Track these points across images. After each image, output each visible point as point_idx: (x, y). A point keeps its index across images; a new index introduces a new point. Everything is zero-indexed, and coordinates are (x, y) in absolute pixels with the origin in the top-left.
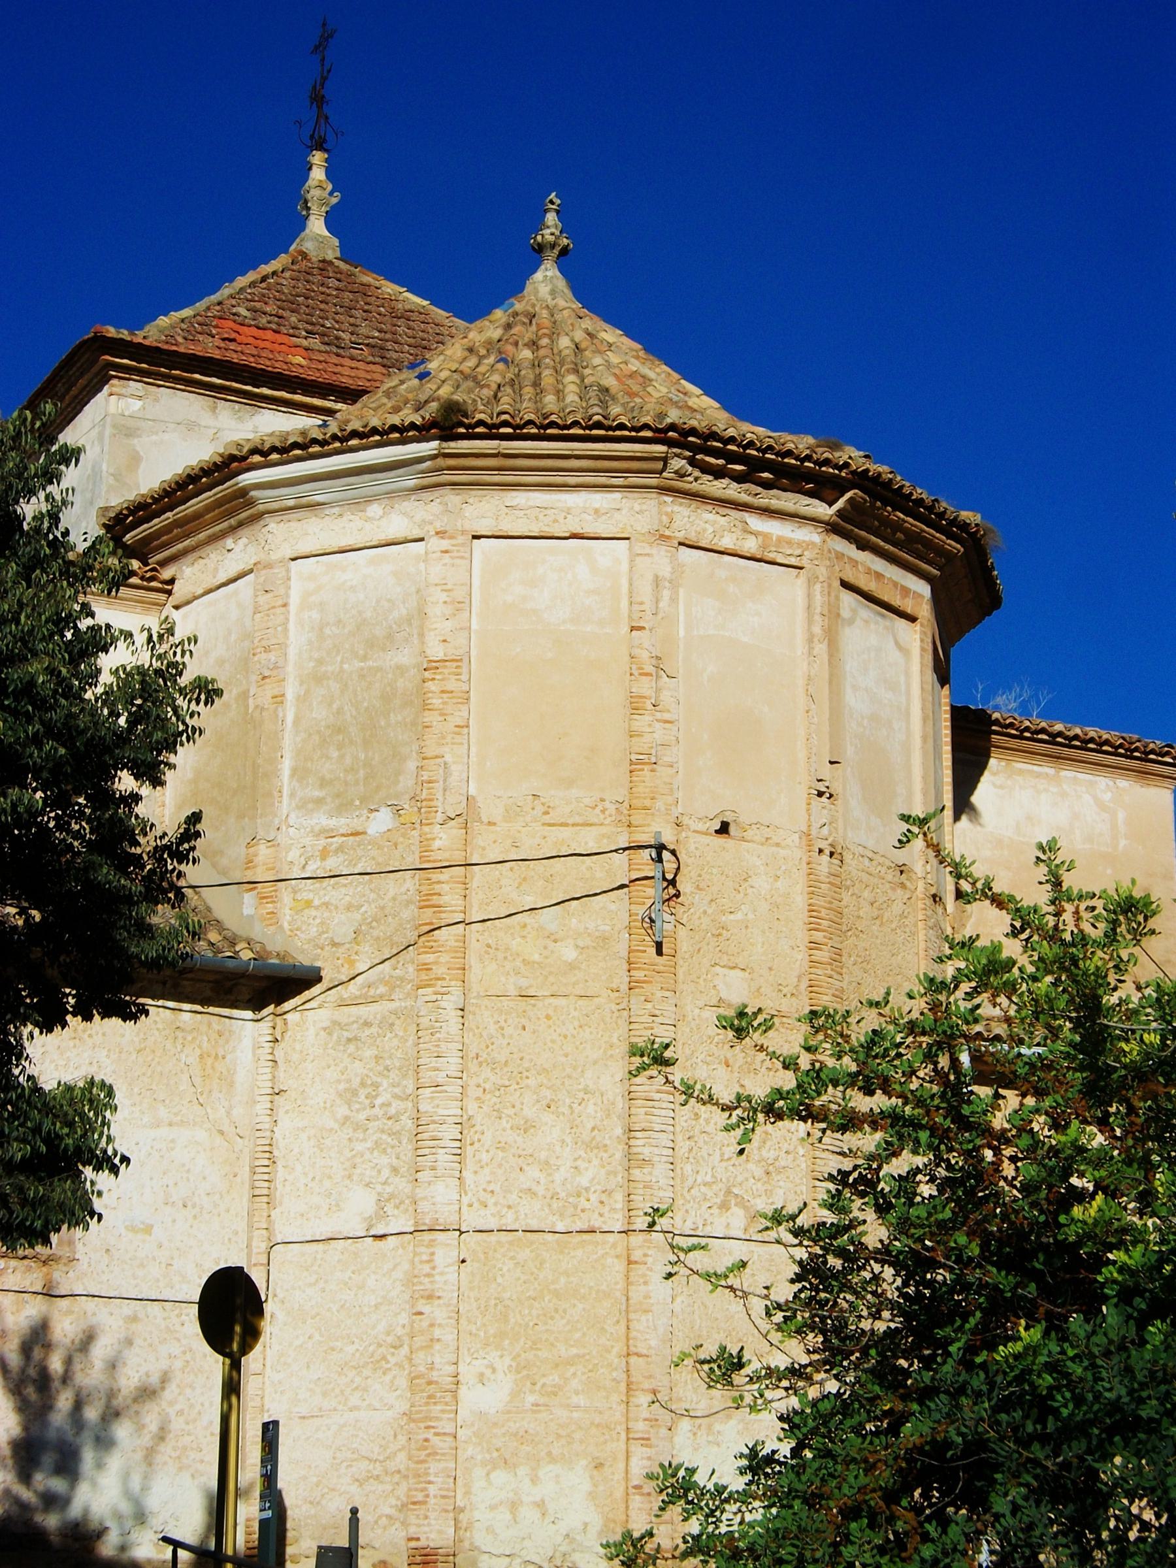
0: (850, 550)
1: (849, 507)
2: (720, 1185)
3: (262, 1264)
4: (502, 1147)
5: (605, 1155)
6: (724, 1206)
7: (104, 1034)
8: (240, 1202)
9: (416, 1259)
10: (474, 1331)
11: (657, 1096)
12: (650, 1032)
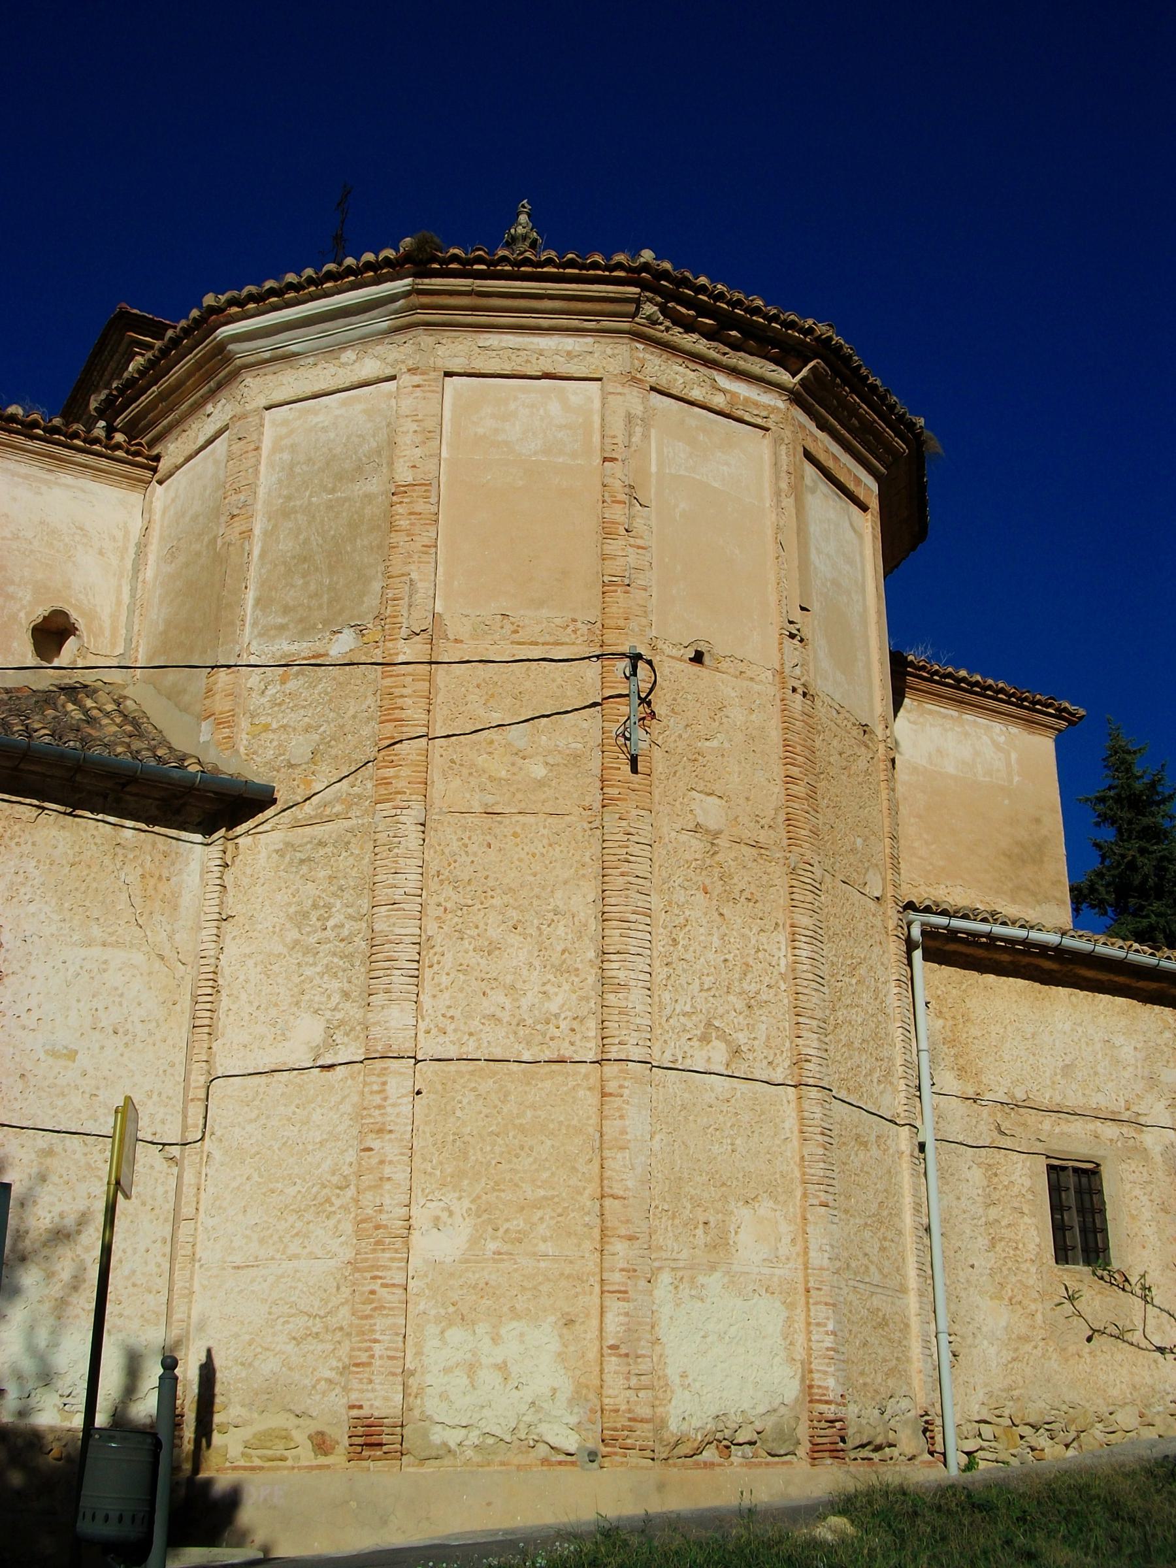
0: (812, 426)
1: (811, 376)
2: (701, 1017)
3: (199, 1099)
4: (463, 969)
5: (576, 980)
6: (705, 1039)
7: (34, 844)
8: (180, 1032)
9: (366, 1090)
10: (429, 1170)
11: (633, 917)
12: (626, 850)
